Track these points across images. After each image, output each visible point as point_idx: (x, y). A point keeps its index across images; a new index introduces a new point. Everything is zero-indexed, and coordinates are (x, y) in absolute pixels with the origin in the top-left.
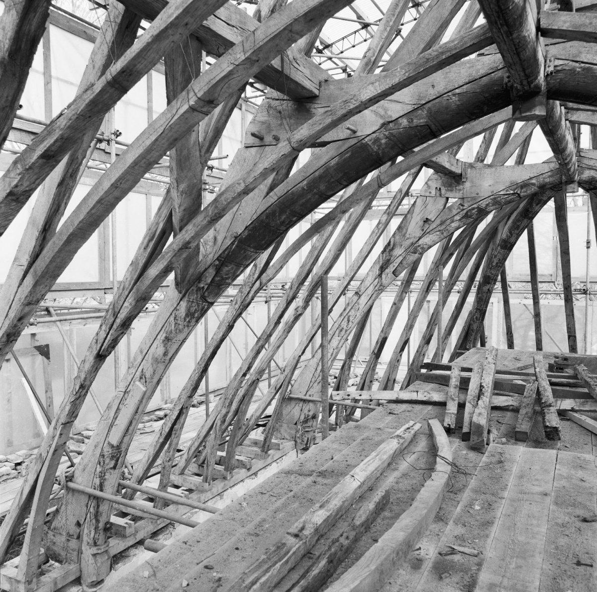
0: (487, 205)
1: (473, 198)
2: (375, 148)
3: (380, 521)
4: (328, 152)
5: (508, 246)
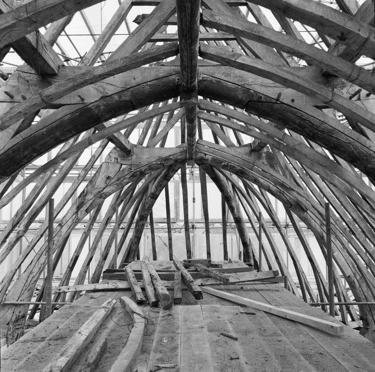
0: (145, 170)
1: (138, 165)
2: (96, 111)
3: (104, 360)
4: (63, 111)
5: (155, 197)
